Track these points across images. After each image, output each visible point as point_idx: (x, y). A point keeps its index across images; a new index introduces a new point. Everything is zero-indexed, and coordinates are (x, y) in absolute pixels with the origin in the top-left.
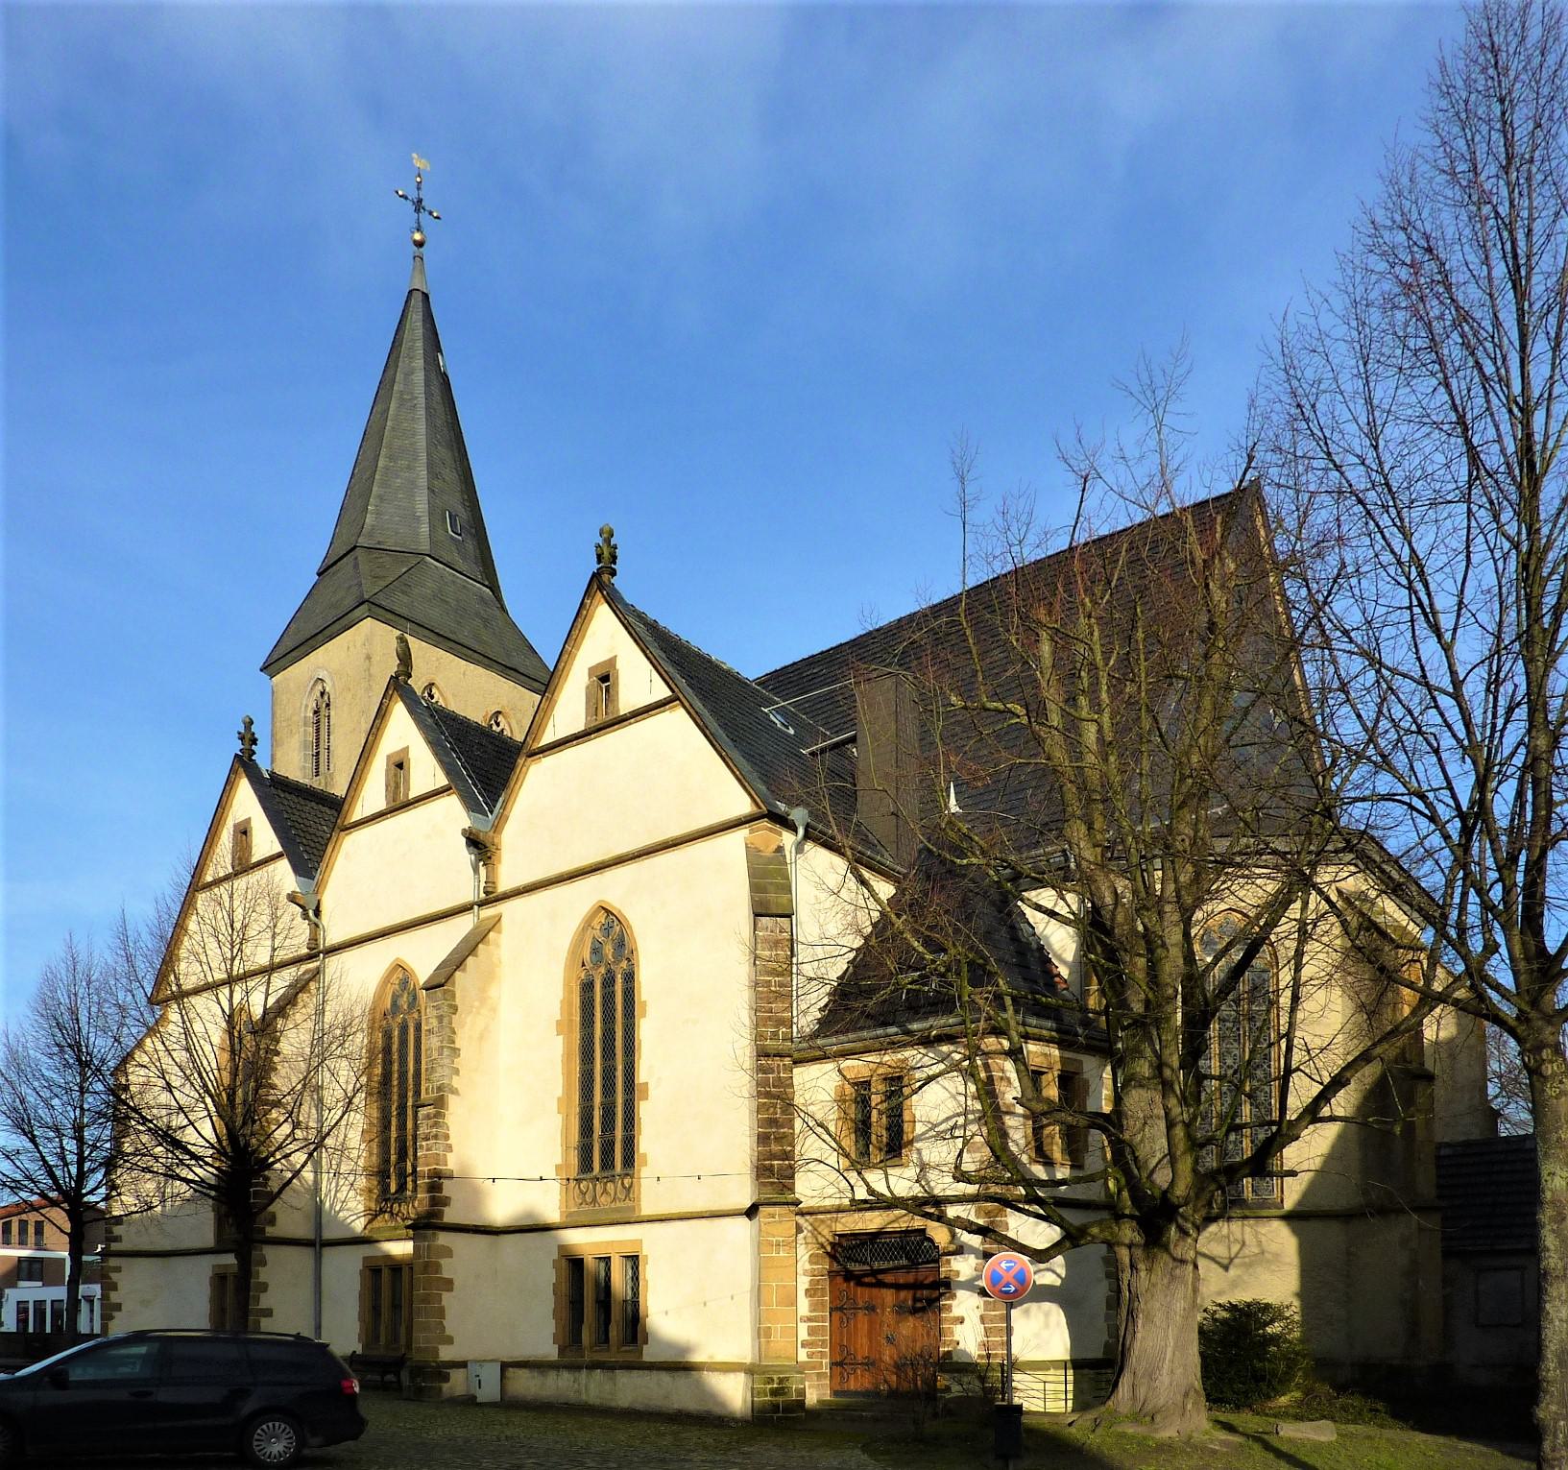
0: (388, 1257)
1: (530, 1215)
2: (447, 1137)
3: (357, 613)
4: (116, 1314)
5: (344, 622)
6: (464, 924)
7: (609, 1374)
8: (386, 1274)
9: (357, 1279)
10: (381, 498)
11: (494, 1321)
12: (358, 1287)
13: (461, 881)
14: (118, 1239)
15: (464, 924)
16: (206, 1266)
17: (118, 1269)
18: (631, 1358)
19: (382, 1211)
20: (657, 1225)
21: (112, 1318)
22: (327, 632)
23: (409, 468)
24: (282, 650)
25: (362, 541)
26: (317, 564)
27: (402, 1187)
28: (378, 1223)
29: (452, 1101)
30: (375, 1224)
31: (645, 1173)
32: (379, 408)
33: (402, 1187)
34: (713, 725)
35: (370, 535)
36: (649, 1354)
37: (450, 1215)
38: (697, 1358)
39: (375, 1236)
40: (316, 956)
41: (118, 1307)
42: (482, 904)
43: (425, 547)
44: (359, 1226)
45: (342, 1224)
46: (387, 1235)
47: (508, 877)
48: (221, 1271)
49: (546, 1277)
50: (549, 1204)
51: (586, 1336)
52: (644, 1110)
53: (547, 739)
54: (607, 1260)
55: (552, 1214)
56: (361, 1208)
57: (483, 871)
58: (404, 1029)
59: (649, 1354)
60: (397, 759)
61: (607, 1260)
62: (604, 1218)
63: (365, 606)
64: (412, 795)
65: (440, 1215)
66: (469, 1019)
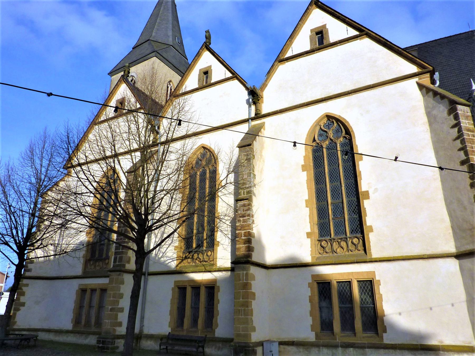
0: (193, 281)
1: (292, 259)
2: (253, 216)
3: (151, 55)
4: (22, 308)
5: (145, 58)
6: (245, 128)
7: (360, 351)
8: (189, 291)
9: (171, 292)
10: (158, 30)
11: (279, 315)
12: (170, 297)
13: (243, 110)
14: (29, 270)
15: (245, 128)
16: (75, 284)
17: (27, 285)
18: (375, 341)
19: (186, 258)
20: (421, 261)
21: (18, 310)
22: (137, 62)
23: (166, 24)
24: (118, 68)
25: (151, 39)
26: (133, 46)
27: (199, 246)
28: (185, 263)
29: (254, 199)
30: (182, 264)
31: (372, 238)
32: (157, 9)
33: (199, 246)
34: (388, 43)
35: (154, 38)
36: (387, 339)
37: (255, 258)
38: (433, 342)
39: (184, 270)
40: (157, 145)
41: (23, 304)
42: (253, 119)
43: (171, 44)
44: (173, 265)
45: (163, 264)
46: (191, 269)
47: (265, 108)
48: (84, 287)
49: (305, 293)
50: (304, 251)
51: (187, 321)
52: (366, 204)
53: (289, 54)
54: (349, 283)
55: (307, 258)
56: (175, 256)
57: (253, 107)
58: (203, 174)
59: (387, 339)
60: (205, 70)
61: (349, 283)
62: (344, 260)
63: (154, 54)
64: (212, 82)
65: (249, 256)
66: (258, 163)
